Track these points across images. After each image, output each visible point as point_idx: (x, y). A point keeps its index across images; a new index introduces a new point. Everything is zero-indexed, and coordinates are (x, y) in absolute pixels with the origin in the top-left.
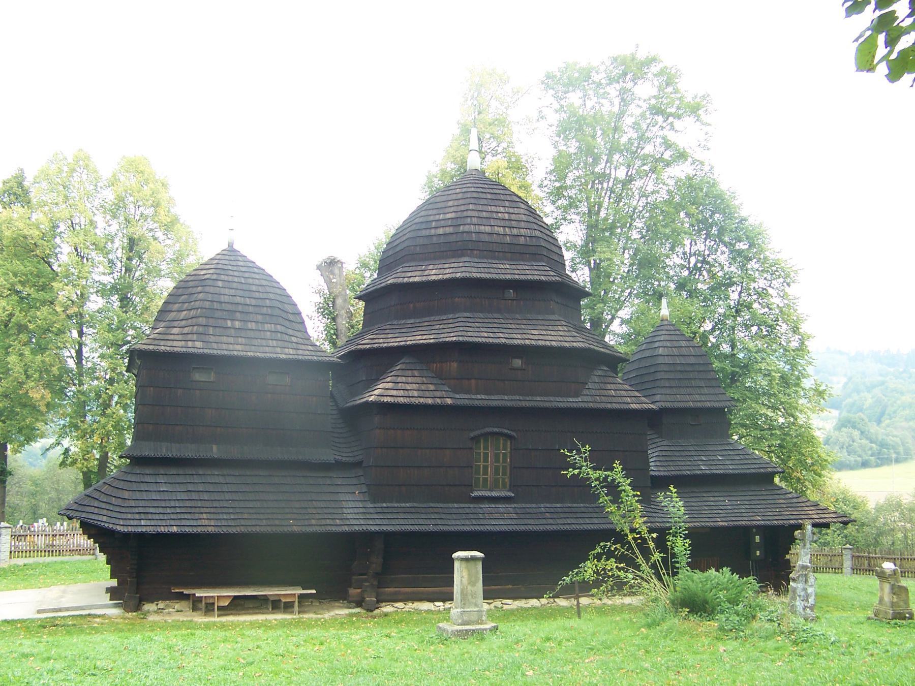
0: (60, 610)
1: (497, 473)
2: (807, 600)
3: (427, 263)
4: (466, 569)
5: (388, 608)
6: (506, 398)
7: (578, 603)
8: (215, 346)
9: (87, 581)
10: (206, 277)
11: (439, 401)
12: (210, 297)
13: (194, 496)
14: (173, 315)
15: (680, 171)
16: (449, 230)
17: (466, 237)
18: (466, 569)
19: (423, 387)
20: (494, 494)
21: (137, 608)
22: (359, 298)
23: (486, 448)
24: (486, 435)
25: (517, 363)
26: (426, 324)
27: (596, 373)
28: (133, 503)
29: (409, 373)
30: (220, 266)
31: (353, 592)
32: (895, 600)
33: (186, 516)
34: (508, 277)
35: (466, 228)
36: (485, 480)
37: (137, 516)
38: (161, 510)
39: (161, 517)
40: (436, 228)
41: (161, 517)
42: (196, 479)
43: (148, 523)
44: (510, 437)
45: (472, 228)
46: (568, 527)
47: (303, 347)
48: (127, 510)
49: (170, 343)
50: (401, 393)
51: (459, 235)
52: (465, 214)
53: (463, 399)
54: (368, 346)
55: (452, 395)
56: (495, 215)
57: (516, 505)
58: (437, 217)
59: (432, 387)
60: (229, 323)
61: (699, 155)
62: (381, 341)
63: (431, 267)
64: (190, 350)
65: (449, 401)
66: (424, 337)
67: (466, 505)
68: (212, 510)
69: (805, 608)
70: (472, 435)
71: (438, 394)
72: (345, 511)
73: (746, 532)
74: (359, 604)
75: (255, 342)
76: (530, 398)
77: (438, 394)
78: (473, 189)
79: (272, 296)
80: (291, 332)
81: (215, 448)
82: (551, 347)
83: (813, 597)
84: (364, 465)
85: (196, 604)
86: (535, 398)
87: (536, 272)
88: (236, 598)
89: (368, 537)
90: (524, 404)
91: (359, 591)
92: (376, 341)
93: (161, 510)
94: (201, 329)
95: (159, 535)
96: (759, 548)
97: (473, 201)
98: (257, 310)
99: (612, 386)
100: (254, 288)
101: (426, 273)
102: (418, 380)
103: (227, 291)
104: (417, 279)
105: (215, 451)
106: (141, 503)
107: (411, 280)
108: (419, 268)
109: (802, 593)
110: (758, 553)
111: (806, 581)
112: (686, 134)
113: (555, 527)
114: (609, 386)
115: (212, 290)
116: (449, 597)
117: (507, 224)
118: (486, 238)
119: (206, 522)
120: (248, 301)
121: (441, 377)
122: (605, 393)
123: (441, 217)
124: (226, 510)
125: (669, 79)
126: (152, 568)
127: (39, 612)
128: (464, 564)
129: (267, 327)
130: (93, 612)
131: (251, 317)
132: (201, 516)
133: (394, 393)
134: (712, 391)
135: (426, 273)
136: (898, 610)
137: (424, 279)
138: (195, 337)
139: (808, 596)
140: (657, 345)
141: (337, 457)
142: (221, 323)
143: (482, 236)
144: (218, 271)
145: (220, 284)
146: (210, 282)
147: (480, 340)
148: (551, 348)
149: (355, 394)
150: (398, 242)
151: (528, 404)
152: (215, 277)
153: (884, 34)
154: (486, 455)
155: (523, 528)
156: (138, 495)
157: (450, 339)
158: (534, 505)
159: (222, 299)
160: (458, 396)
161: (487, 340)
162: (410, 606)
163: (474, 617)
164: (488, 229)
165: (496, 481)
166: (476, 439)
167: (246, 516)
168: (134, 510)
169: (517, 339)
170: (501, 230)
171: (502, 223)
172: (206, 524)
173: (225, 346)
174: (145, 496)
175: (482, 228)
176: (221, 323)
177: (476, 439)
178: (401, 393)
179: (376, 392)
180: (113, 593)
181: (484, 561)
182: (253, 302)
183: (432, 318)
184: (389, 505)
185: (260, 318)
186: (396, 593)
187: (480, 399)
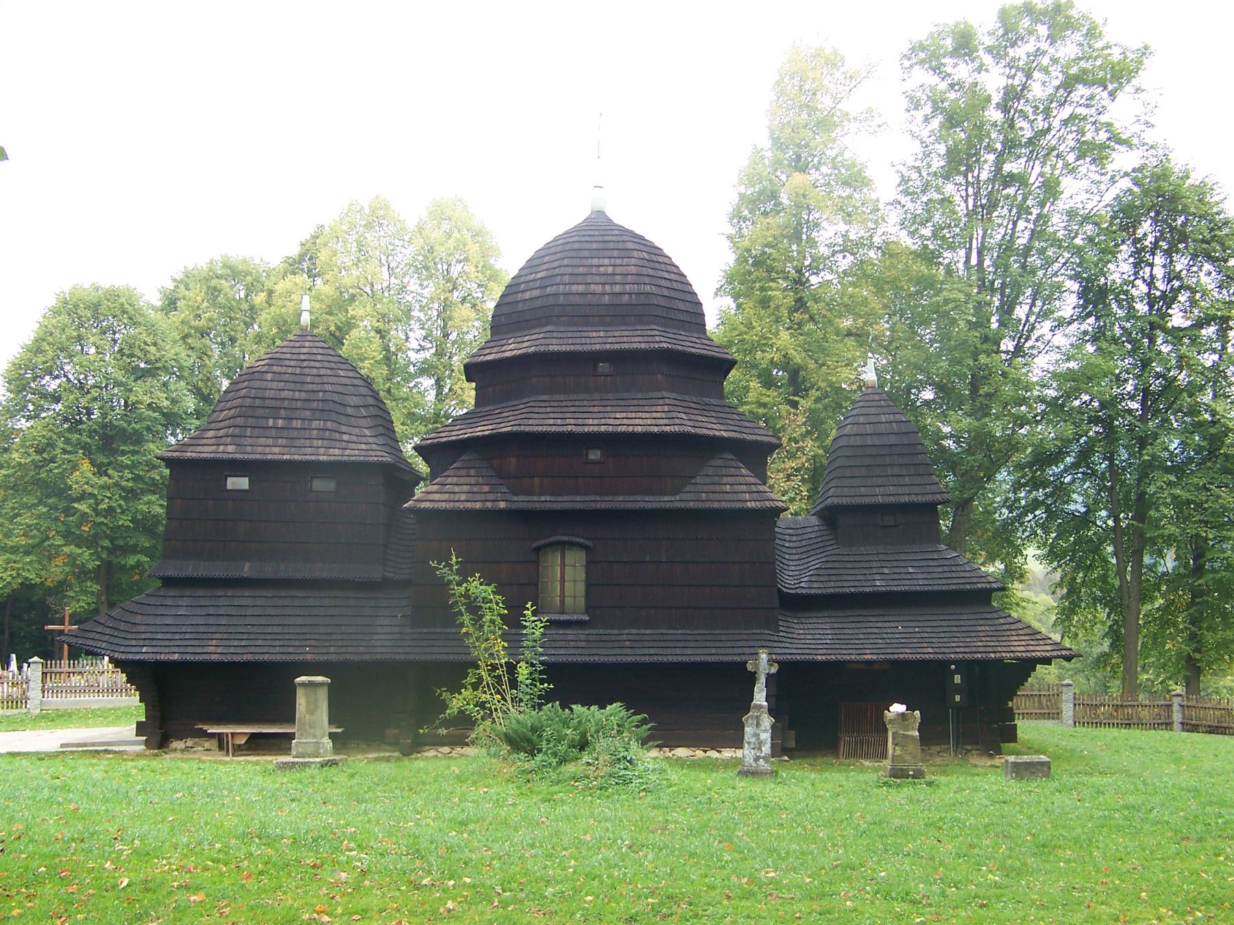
0: (85, 745)
2: (760, 749)
6: (578, 498)
8: (249, 449)
9: (104, 709)
11: (489, 505)
13: (212, 621)
15: (1123, 160)
16: (536, 293)
17: (551, 301)
18: (312, 706)
19: (475, 489)
24: (552, 545)
25: (595, 455)
27: (713, 463)
28: (142, 629)
29: (464, 472)
31: (390, 732)
32: (898, 753)
33: (194, 643)
34: (598, 347)
38: (169, 636)
39: (167, 643)
40: (523, 291)
41: (167, 643)
42: (221, 602)
43: (151, 649)
46: (647, 659)
47: (353, 446)
48: (133, 636)
50: (446, 496)
52: (557, 271)
53: (522, 501)
55: (509, 497)
56: (594, 270)
57: (591, 631)
61: (1150, 137)
65: (502, 505)
70: (534, 545)
71: (491, 497)
75: (297, 443)
76: (610, 498)
77: (491, 497)
79: (328, 387)
80: (344, 429)
82: (634, 434)
83: (769, 745)
85: (222, 743)
86: (617, 498)
87: (637, 339)
88: (253, 736)
90: (598, 506)
93: (169, 636)
94: (237, 431)
98: (306, 405)
99: (730, 480)
102: (473, 480)
105: (247, 570)
106: (151, 629)
109: (753, 740)
110: (958, 698)
111: (758, 725)
112: (1122, 111)
113: (633, 659)
114: (725, 480)
117: (609, 279)
118: (578, 300)
122: (717, 488)
125: (1092, 33)
127: (62, 746)
129: (315, 424)
130: (110, 748)
131: (297, 414)
132: (210, 643)
133: (437, 497)
134: (918, 480)
136: (900, 765)
139: (761, 743)
142: (262, 422)
143: (571, 297)
147: (545, 429)
148: (634, 435)
151: (604, 506)
156: (151, 620)
158: (615, 632)
159: (268, 394)
160: (515, 498)
161: (554, 429)
163: (310, 750)
164: (581, 288)
166: (538, 550)
167: (260, 643)
169: (593, 424)
171: (603, 279)
172: (214, 652)
173: (260, 449)
174: (159, 621)
176: (262, 422)
177: (538, 550)
178: (446, 496)
180: (141, 728)
181: (329, 685)
182: (303, 396)
184: (432, 630)
185: (308, 413)
187: (545, 501)
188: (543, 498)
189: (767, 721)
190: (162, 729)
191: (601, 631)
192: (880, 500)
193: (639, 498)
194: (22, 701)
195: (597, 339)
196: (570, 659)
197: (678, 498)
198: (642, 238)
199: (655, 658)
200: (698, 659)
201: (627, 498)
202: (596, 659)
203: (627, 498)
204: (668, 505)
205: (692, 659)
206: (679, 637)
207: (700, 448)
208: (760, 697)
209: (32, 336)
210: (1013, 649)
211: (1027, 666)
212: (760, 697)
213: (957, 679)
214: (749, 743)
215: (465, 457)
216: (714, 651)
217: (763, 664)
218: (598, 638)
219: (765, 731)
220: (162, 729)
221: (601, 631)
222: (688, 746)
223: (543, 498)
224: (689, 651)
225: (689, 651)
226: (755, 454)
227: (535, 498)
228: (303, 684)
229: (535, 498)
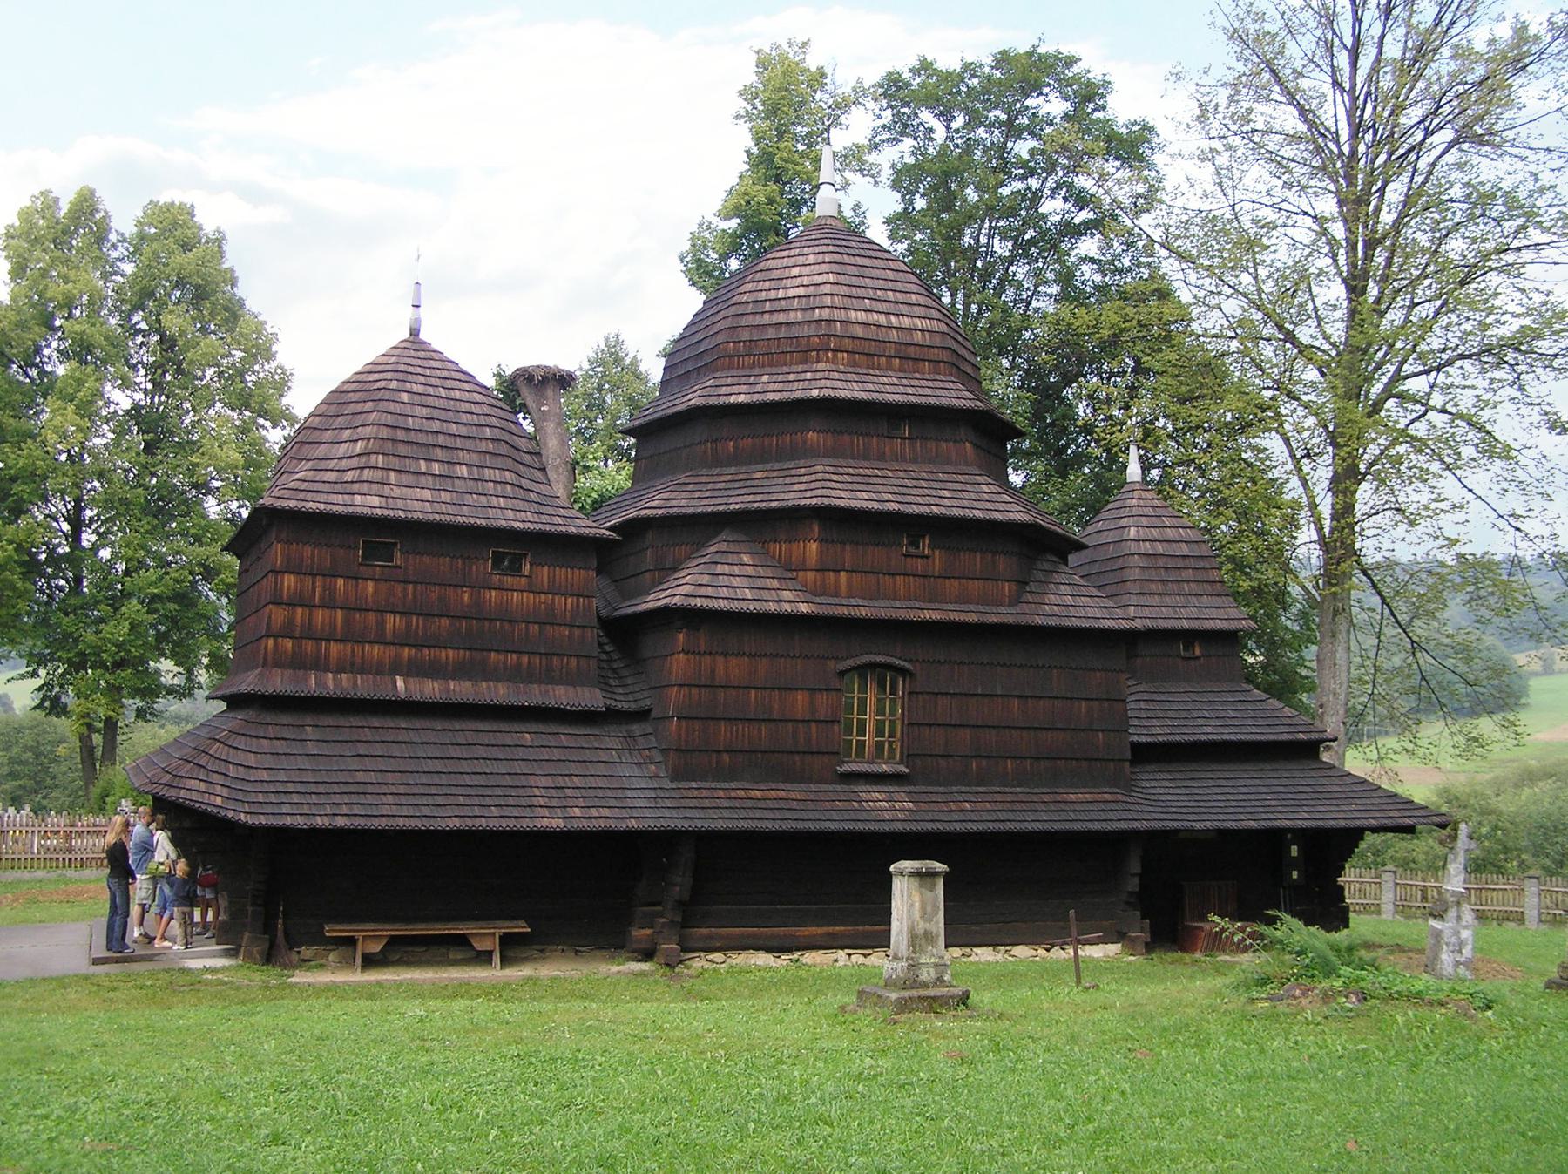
1: (880, 732)
3: (757, 371)
4: (913, 900)
5: (698, 963)
7: (1076, 953)
10: (378, 385)
12: (389, 420)
14: (321, 451)
18: (913, 900)
20: (875, 769)
21: (269, 958)
22: (628, 432)
23: (863, 689)
26: (759, 475)
28: (264, 775)
30: (402, 368)
35: (826, 313)
36: (861, 744)
37: (273, 798)
44: (902, 671)
45: (837, 314)
49: (324, 497)
51: (813, 326)
54: (660, 512)
57: (912, 788)
58: (773, 295)
59: (775, 584)
60: (423, 466)
62: (683, 503)
63: (765, 378)
64: (359, 510)
66: (759, 498)
67: (831, 788)
68: (402, 789)
69: (1457, 964)
72: (629, 793)
73: (1273, 839)
74: (648, 955)
78: (831, 248)
81: (400, 683)
83: (1469, 947)
84: (653, 714)
89: (666, 841)
91: (649, 931)
92: (674, 503)
95: (314, 832)
96: (1250, 868)
97: (835, 268)
100: (464, 407)
101: (759, 388)
103: (418, 411)
104: (741, 399)
107: (732, 399)
108: (743, 380)
110: (1295, 874)
115: (392, 407)
116: (881, 941)
119: (395, 810)
120: (453, 428)
121: (789, 569)
123: (781, 294)
124: (394, 789)
126: (285, 888)
128: (915, 882)
132: (385, 799)
135: (759, 388)
137: (755, 398)
138: (365, 488)
139: (1461, 944)
140: (1124, 522)
141: (608, 702)
142: (410, 465)
144: (401, 376)
145: (405, 397)
146: (387, 395)
149: (627, 595)
150: (699, 336)
152: (394, 385)
153: (303, 401)
154: (862, 703)
155: (930, 827)
157: (808, 502)
162: (738, 959)
165: (879, 747)
168: (266, 787)
170: (882, 319)
171: (885, 307)
175: (853, 315)
176: (410, 465)
179: (680, 590)
183: (769, 466)
186: (710, 937)
192: (1186, 624)
195: (891, 388)
209: (251, 305)
210: (629, 803)
211: (1356, 835)
213: (1294, 851)
215: (723, 536)
219: (1466, 927)
222: (994, 945)
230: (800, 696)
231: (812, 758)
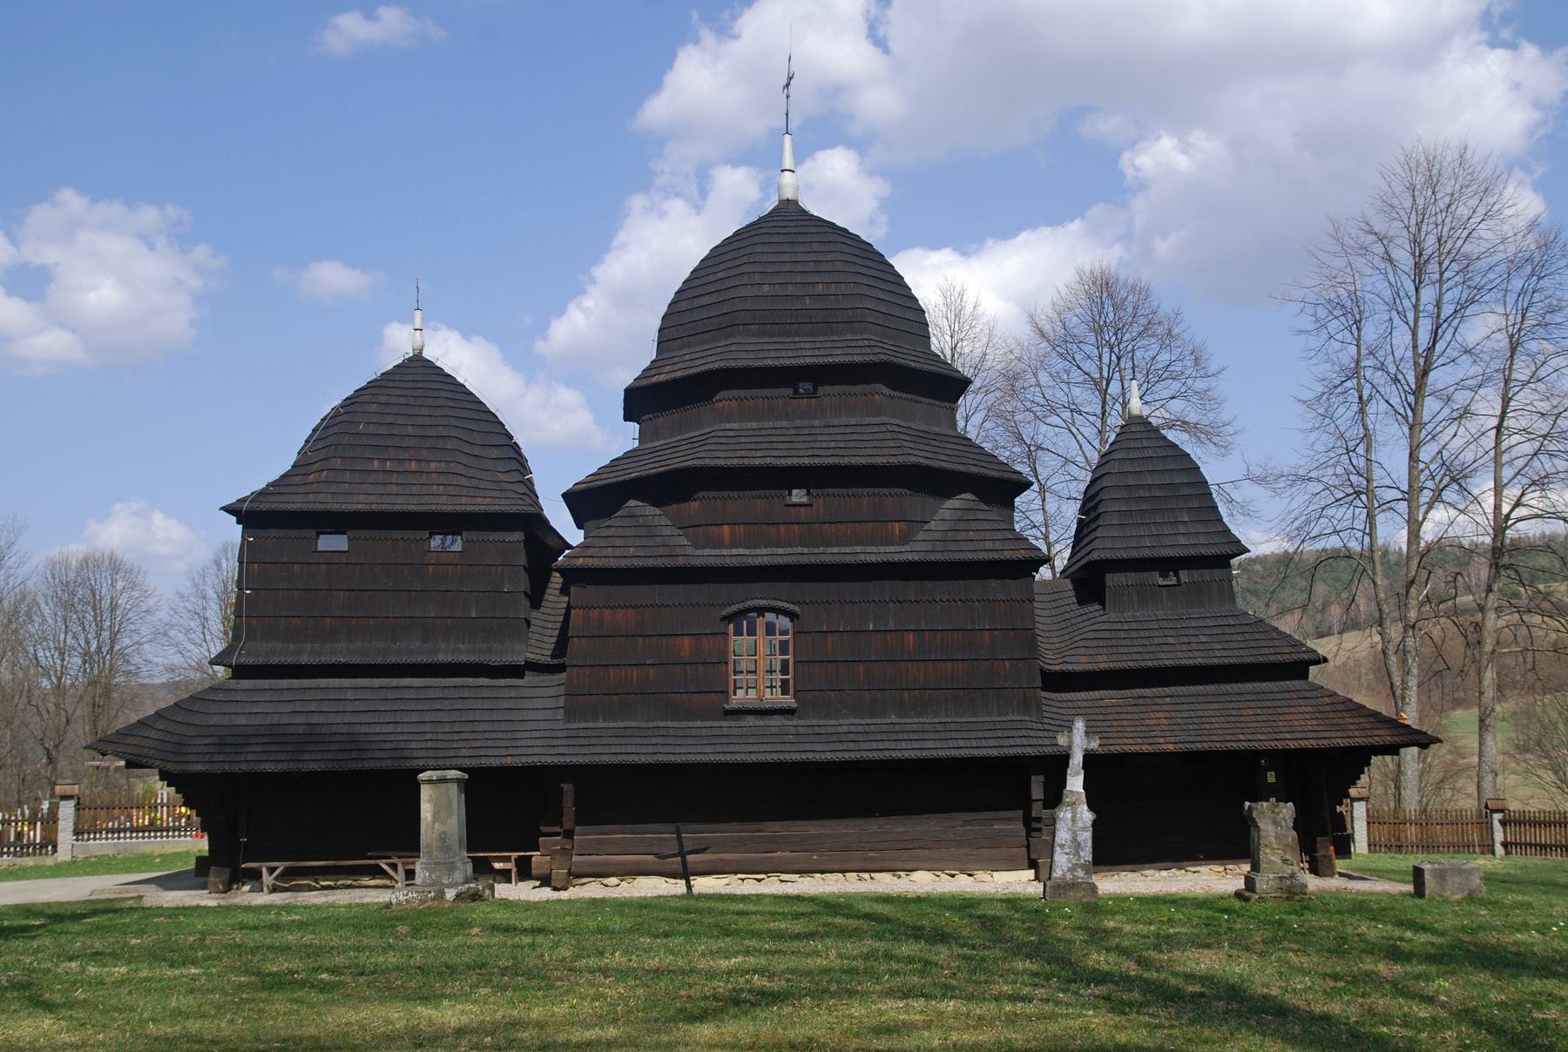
6: (780, 551)
25: (798, 496)
57: (802, 722)
70: (724, 613)
86: (830, 550)
188: (735, 551)
189: (1086, 816)
190: (227, 863)
191: (814, 722)
193: (858, 549)
194: (49, 843)
196: (776, 757)
197: (908, 548)
198: (845, 230)
199: (887, 754)
200: (942, 753)
201: (843, 550)
202: (811, 756)
203: (843, 550)
204: (896, 558)
205: (935, 754)
206: (915, 727)
207: (935, 482)
208: (1075, 783)
212: (1075, 783)
213: (1271, 777)
214: (1062, 846)
216: (961, 743)
217: (1079, 742)
218: (810, 730)
219: (1083, 829)
220: (227, 863)
221: (814, 722)
223: (735, 551)
224: (930, 744)
225: (930, 744)
226: (1002, 488)
227: (725, 552)
228: (430, 782)
229: (725, 552)
230: (686, 641)
231: (704, 689)
